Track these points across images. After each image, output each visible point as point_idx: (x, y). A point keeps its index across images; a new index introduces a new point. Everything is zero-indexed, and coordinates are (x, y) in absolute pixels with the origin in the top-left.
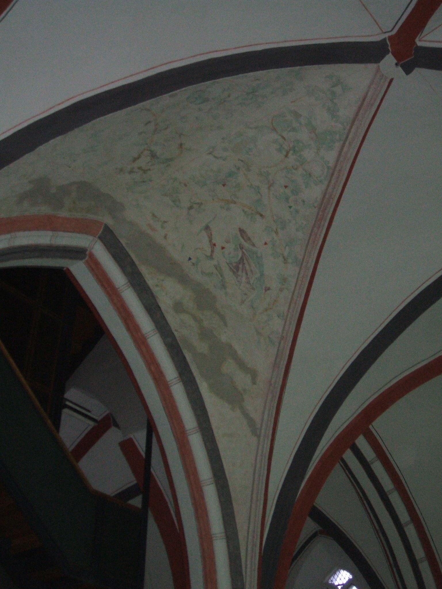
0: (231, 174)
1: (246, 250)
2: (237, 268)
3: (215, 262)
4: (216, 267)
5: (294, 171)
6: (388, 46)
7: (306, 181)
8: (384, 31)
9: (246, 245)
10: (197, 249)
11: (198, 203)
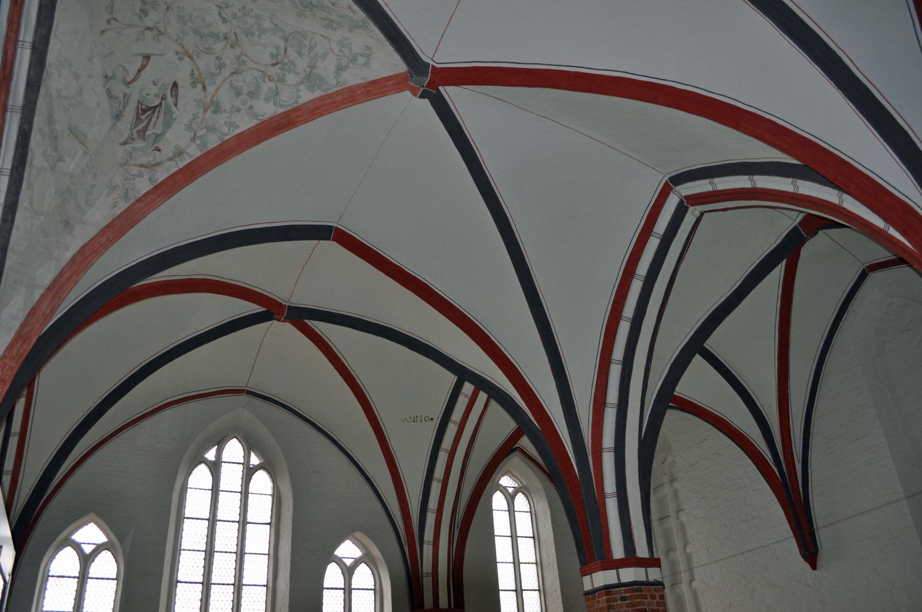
0: (215, 36)
2: (144, 112)
3: (127, 91)
4: (125, 94)
5: (267, 80)
7: (269, 95)
10: (122, 66)
11: (160, 31)
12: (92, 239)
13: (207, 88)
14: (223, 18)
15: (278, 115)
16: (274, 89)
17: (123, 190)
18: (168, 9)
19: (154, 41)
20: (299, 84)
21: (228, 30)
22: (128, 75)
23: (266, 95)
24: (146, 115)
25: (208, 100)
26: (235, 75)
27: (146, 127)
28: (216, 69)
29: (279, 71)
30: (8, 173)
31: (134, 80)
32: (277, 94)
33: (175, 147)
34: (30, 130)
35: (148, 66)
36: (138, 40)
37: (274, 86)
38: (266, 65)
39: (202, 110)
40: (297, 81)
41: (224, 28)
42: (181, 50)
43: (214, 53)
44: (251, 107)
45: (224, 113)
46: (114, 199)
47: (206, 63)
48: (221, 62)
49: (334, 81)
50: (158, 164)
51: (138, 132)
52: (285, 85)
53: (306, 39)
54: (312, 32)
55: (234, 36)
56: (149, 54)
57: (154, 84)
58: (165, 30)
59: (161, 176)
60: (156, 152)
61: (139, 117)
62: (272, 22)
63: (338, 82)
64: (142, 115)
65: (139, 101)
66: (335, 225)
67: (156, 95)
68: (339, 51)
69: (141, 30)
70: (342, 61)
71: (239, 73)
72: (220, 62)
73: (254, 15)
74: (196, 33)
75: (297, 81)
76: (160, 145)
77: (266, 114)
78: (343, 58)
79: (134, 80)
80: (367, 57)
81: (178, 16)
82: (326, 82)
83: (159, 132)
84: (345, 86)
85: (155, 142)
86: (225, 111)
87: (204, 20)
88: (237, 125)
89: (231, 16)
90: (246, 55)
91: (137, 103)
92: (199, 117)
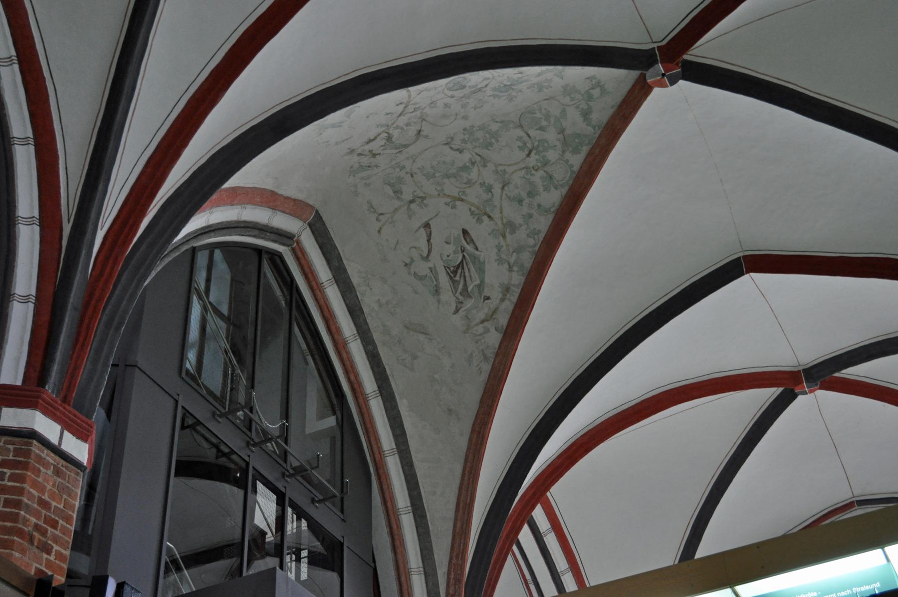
0: (464, 168)
1: (467, 254)
2: (455, 272)
3: (431, 265)
4: (430, 269)
5: (533, 172)
6: (656, 55)
7: (545, 183)
8: (654, 41)
9: (469, 248)
10: (412, 247)
11: (421, 197)
12: (477, 414)
13: (492, 216)
14: (458, 150)
15: (565, 196)
16: (545, 176)
17: (479, 353)
18: (412, 176)
19: (422, 208)
20: (562, 155)
21: (470, 156)
22: (422, 251)
23: (543, 186)
24: (458, 275)
25: (501, 226)
26: (506, 188)
27: (465, 285)
28: (488, 194)
29: (537, 157)
30: (378, 393)
31: (430, 252)
32: (551, 177)
33: (499, 287)
34: (375, 347)
35: (432, 232)
36: (410, 217)
37: (544, 173)
38: (523, 160)
39: (501, 238)
40: (559, 154)
41: (466, 157)
42: (448, 200)
43: (476, 182)
44: (539, 206)
45: (521, 227)
46: (477, 366)
47: (475, 195)
48: (487, 185)
49: (590, 129)
50: (495, 312)
51: (461, 294)
52: (552, 164)
53: (536, 114)
54: (534, 104)
55: (477, 156)
56: (426, 222)
57: (447, 243)
58: (424, 193)
59: (503, 320)
60: (486, 301)
61: (454, 280)
62: (497, 122)
63: (594, 127)
64: (455, 276)
65: (445, 267)
66: (741, 255)
67: (455, 252)
68: (571, 100)
69: (407, 206)
70: (581, 106)
71: (508, 183)
72: (486, 186)
73: (478, 129)
74: (448, 178)
75: (559, 154)
76: (486, 293)
77: (555, 203)
78: (579, 103)
79: (430, 252)
80: (598, 86)
81: (424, 175)
82: (584, 135)
83: (478, 282)
84: (603, 126)
85: (480, 293)
86: (521, 225)
87: (444, 163)
88: (538, 230)
89: (462, 143)
90: (500, 165)
91: (444, 269)
92: (502, 246)
